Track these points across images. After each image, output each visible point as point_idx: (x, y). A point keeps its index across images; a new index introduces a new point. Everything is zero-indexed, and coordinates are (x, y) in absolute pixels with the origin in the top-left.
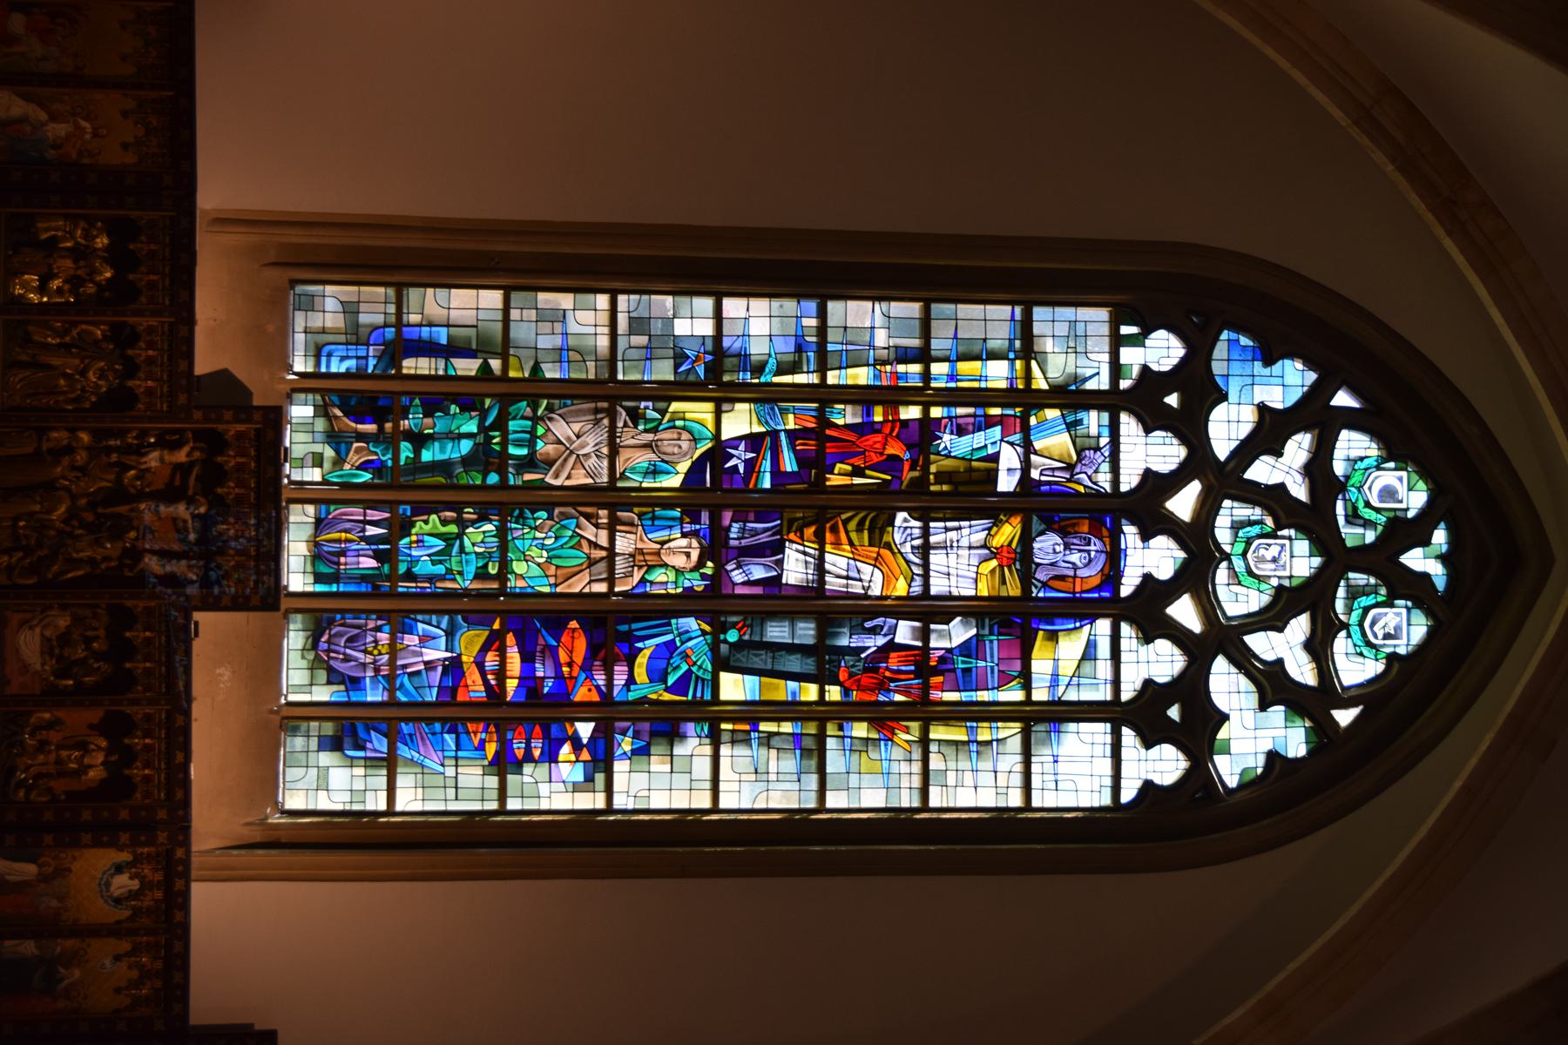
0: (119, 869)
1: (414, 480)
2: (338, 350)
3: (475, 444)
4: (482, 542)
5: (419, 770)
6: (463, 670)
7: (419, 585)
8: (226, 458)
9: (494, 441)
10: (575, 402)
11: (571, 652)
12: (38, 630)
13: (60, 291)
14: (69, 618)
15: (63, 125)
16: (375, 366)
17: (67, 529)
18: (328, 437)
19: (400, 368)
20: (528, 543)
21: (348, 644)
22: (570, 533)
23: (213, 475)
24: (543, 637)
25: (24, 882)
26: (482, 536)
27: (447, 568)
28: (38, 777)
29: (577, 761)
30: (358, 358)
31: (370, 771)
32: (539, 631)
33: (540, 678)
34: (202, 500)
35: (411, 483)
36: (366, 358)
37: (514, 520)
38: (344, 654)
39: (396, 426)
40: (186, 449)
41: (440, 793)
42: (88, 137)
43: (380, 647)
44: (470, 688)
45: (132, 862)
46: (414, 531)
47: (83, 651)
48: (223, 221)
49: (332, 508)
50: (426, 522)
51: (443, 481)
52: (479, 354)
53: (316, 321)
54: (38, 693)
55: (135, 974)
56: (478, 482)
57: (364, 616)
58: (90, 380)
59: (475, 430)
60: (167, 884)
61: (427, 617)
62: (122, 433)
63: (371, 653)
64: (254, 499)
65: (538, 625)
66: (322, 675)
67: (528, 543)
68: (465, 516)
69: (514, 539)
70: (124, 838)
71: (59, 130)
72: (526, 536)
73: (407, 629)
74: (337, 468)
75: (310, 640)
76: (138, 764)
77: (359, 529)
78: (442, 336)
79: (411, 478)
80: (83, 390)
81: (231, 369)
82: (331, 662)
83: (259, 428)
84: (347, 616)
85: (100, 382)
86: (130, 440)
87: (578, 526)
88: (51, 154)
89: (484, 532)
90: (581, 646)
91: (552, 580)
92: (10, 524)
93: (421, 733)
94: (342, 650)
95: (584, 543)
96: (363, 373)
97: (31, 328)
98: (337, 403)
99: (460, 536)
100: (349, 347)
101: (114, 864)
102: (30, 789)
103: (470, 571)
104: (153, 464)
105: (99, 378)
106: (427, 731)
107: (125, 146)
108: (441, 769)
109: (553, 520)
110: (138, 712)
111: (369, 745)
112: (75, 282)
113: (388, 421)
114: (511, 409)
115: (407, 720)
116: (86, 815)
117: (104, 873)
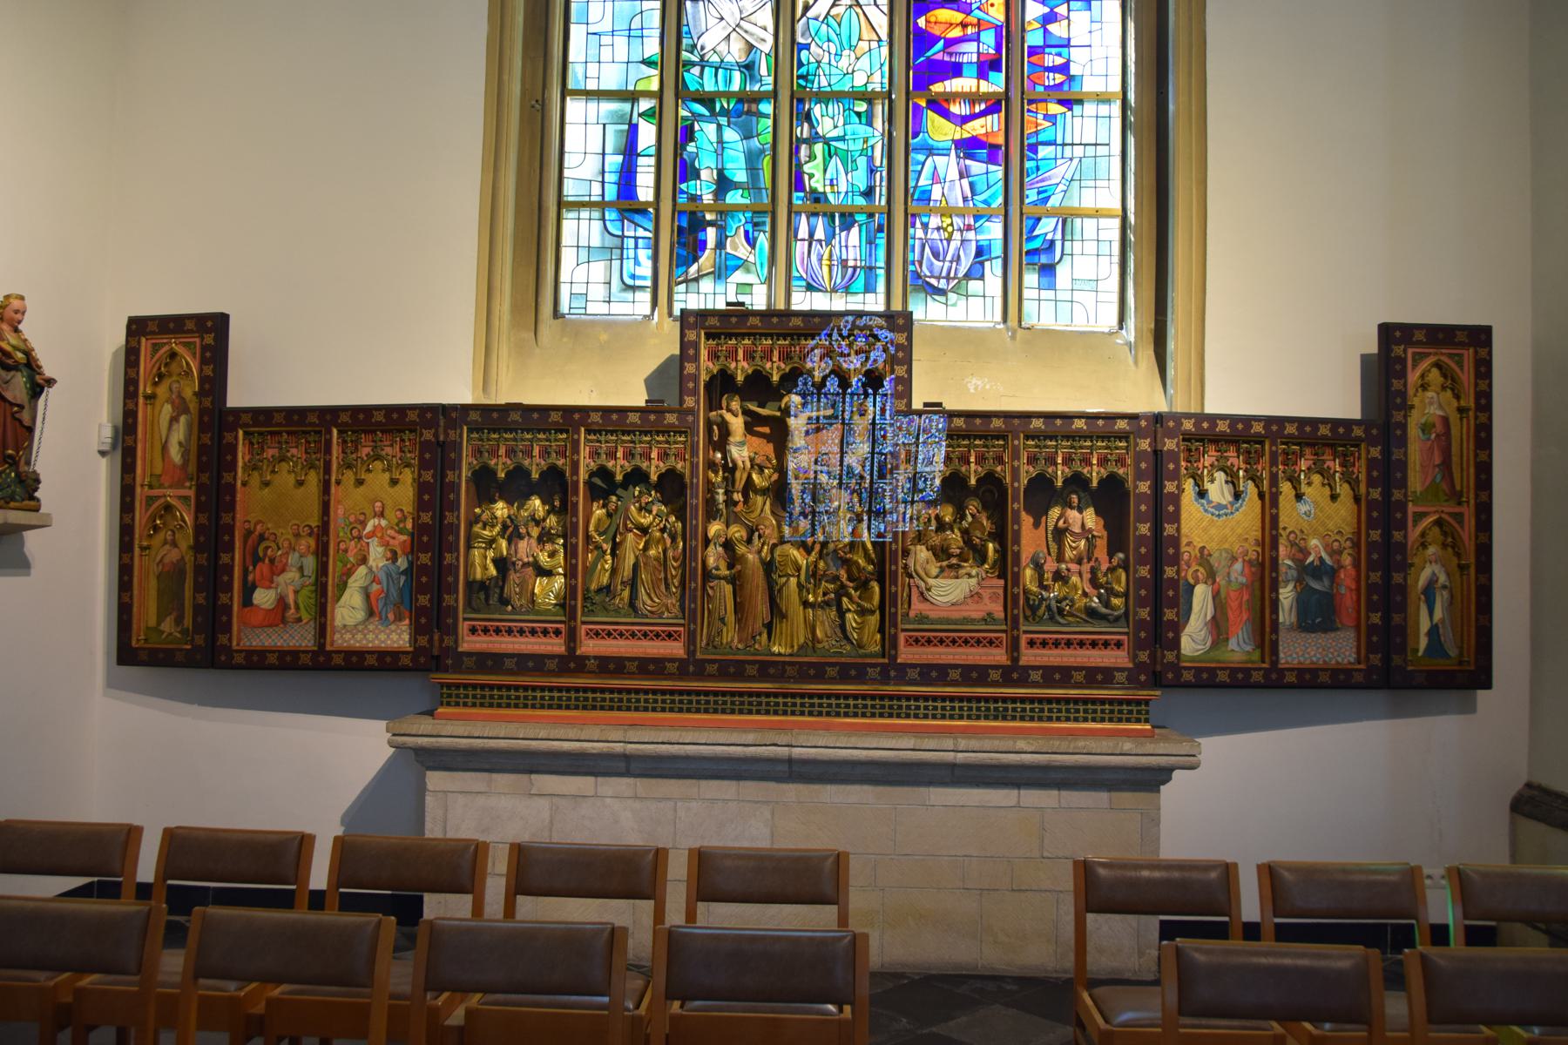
0: (1202, 494)
1: (766, 189)
2: (628, 268)
3: (729, 126)
4: (833, 118)
5: (1076, 184)
6: (969, 138)
7: (878, 184)
8: (739, 371)
9: (726, 106)
10: (685, 23)
11: (951, 24)
12: (931, 581)
13: (552, 555)
14: (919, 547)
15: (371, 549)
16: (645, 229)
17: (817, 547)
18: (719, 277)
19: (648, 203)
20: (834, 71)
21: (941, 258)
22: (824, 26)
23: (759, 387)
24: (934, 54)
25: (1214, 598)
26: (826, 118)
27: (861, 155)
28: (1094, 582)
29: (1068, 18)
30: (636, 247)
31: (1077, 236)
32: (928, 58)
33: (978, 58)
34: (786, 399)
35: (769, 192)
36: (636, 238)
37: (809, 85)
38: (951, 262)
39: (710, 209)
40: (728, 417)
41: (1102, 162)
42: (384, 523)
43: (945, 225)
44: (989, 130)
45: (1195, 480)
46: (821, 189)
47: (953, 532)
48: (486, 380)
49: (795, 274)
50: (811, 176)
51: (768, 158)
52: (634, 121)
53: (597, 292)
54: (1002, 582)
55: (1317, 478)
56: (770, 122)
57: (911, 242)
58: (651, 523)
59: (714, 126)
60: (1217, 440)
61: (912, 176)
62: (710, 487)
63: (951, 234)
64: (785, 340)
65: (922, 59)
66: (974, 286)
67: (834, 71)
68: (805, 136)
69: (830, 85)
70: (1170, 487)
71: (377, 555)
72: (827, 72)
73: (926, 196)
74: (753, 268)
75: (936, 297)
76: (1085, 471)
77: (819, 246)
78: (614, 161)
79: (764, 191)
80: (663, 530)
81: (645, 376)
82: (960, 275)
83: (705, 334)
84: (910, 258)
85: (654, 512)
86: (719, 479)
87: (816, 19)
88: (402, 563)
89: (822, 116)
90: (944, 14)
91: (874, 45)
92: (810, 610)
93: (1037, 182)
94: (947, 264)
95: (834, 12)
96: (652, 242)
97: (593, 586)
98: (684, 269)
99: (827, 142)
100: (625, 256)
101: (1196, 500)
102: (1111, 592)
103: (863, 130)
104: (745, 453)
105: (650, 512)
106: (1034, 176)
107: (394, 482)
108: (1076, 161)
109: (810, 44)
110: (1027, 472)
111: (1049, 237)
112: (545, 537)
113: (704, 216)
114: (692, 88)
115: (1022, 197)
116: (1144, 529)
117: (1206, 511)
